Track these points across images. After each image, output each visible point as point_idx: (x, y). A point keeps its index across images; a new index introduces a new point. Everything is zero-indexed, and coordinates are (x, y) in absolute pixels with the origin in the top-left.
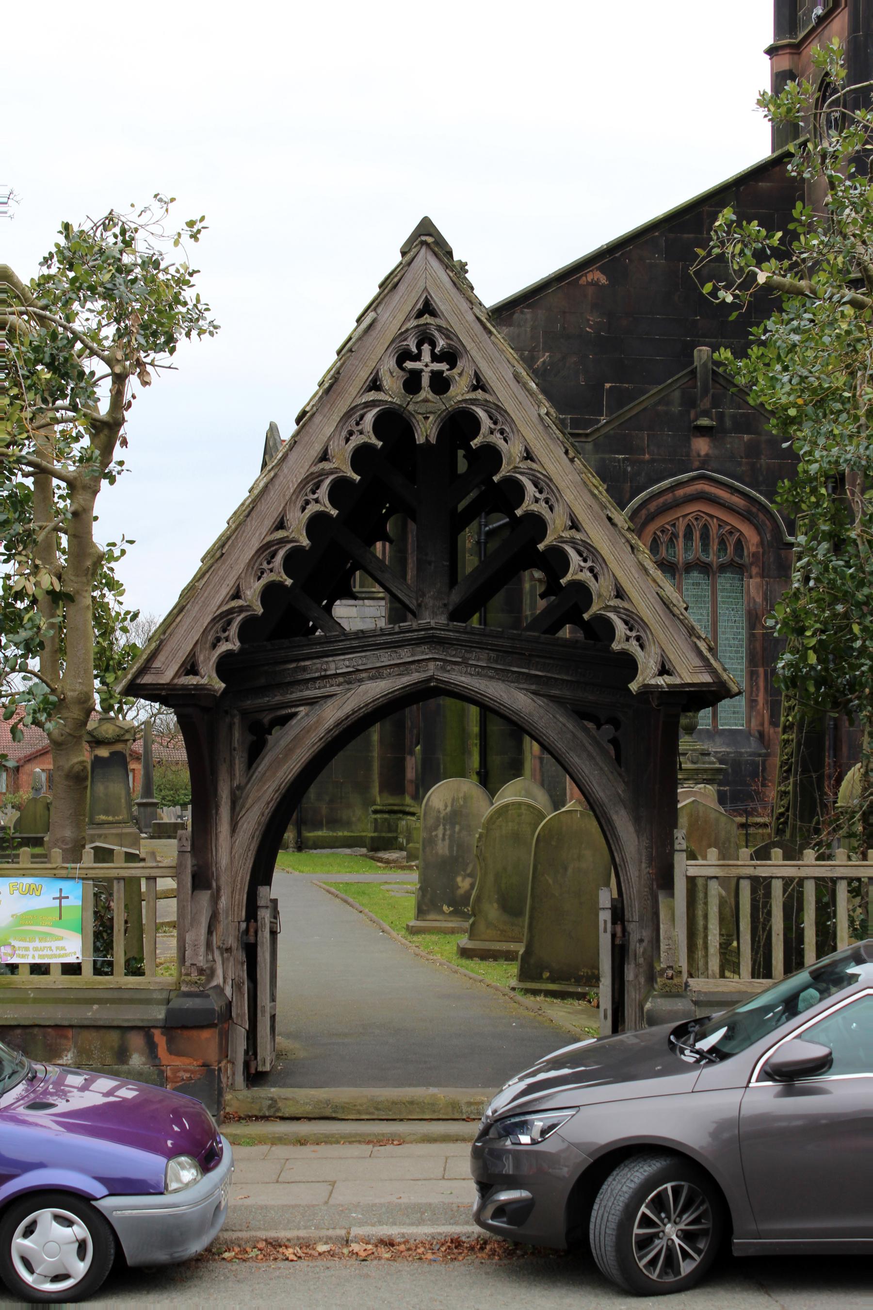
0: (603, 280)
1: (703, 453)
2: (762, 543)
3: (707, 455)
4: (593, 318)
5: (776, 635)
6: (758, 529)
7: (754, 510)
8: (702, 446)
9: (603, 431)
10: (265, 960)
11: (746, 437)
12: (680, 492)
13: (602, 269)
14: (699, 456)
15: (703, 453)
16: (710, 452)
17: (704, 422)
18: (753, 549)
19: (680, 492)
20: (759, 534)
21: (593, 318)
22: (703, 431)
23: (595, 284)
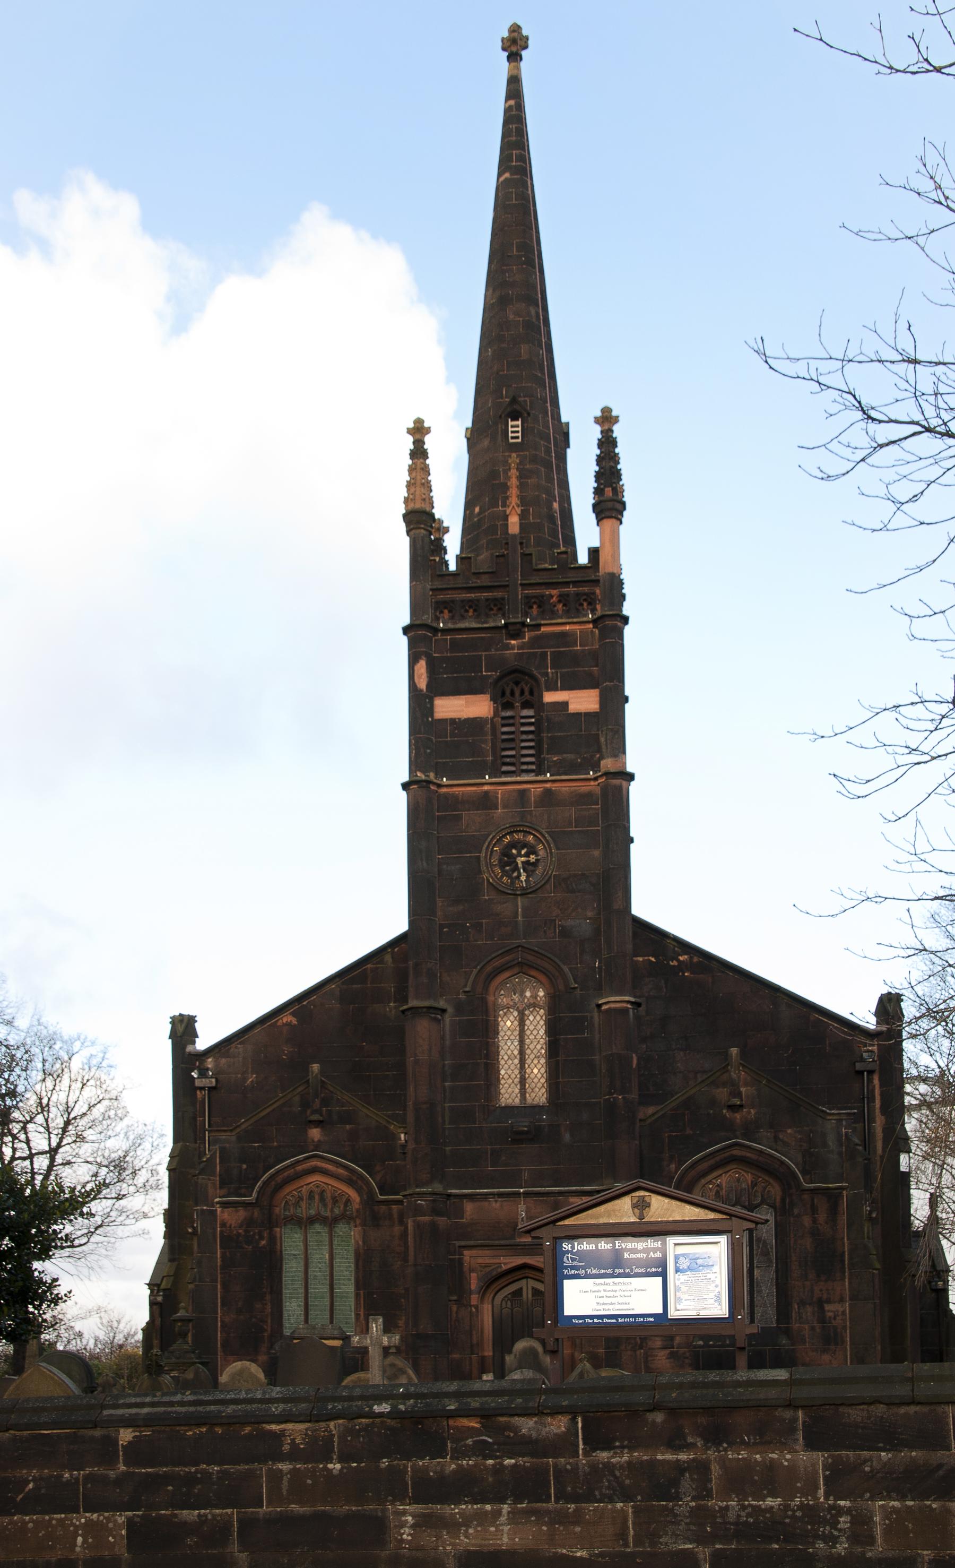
0: (294, 1021)
1: (316, 1140)
2: (361, 1202)
3: (319, 1141)
4: (287, 1049)
5: (31, 1308)
6: (359, 1191)
7: (355, 1178)
8: (315, 1133)
9: (243, 1127)
10: (694, 1385)
11: (348, 1127)
12: (299, 1168)
13: (293, 1014)
14: (313, 1141)
15: (316, 1140)
16: (322, 1139)
17: (316, 1117)
18: (357, 1206)
19: (299, 1168)
20: (360, 1195)
21: (287, 1049)
22: (318, 1124)
23: (288, 1024)
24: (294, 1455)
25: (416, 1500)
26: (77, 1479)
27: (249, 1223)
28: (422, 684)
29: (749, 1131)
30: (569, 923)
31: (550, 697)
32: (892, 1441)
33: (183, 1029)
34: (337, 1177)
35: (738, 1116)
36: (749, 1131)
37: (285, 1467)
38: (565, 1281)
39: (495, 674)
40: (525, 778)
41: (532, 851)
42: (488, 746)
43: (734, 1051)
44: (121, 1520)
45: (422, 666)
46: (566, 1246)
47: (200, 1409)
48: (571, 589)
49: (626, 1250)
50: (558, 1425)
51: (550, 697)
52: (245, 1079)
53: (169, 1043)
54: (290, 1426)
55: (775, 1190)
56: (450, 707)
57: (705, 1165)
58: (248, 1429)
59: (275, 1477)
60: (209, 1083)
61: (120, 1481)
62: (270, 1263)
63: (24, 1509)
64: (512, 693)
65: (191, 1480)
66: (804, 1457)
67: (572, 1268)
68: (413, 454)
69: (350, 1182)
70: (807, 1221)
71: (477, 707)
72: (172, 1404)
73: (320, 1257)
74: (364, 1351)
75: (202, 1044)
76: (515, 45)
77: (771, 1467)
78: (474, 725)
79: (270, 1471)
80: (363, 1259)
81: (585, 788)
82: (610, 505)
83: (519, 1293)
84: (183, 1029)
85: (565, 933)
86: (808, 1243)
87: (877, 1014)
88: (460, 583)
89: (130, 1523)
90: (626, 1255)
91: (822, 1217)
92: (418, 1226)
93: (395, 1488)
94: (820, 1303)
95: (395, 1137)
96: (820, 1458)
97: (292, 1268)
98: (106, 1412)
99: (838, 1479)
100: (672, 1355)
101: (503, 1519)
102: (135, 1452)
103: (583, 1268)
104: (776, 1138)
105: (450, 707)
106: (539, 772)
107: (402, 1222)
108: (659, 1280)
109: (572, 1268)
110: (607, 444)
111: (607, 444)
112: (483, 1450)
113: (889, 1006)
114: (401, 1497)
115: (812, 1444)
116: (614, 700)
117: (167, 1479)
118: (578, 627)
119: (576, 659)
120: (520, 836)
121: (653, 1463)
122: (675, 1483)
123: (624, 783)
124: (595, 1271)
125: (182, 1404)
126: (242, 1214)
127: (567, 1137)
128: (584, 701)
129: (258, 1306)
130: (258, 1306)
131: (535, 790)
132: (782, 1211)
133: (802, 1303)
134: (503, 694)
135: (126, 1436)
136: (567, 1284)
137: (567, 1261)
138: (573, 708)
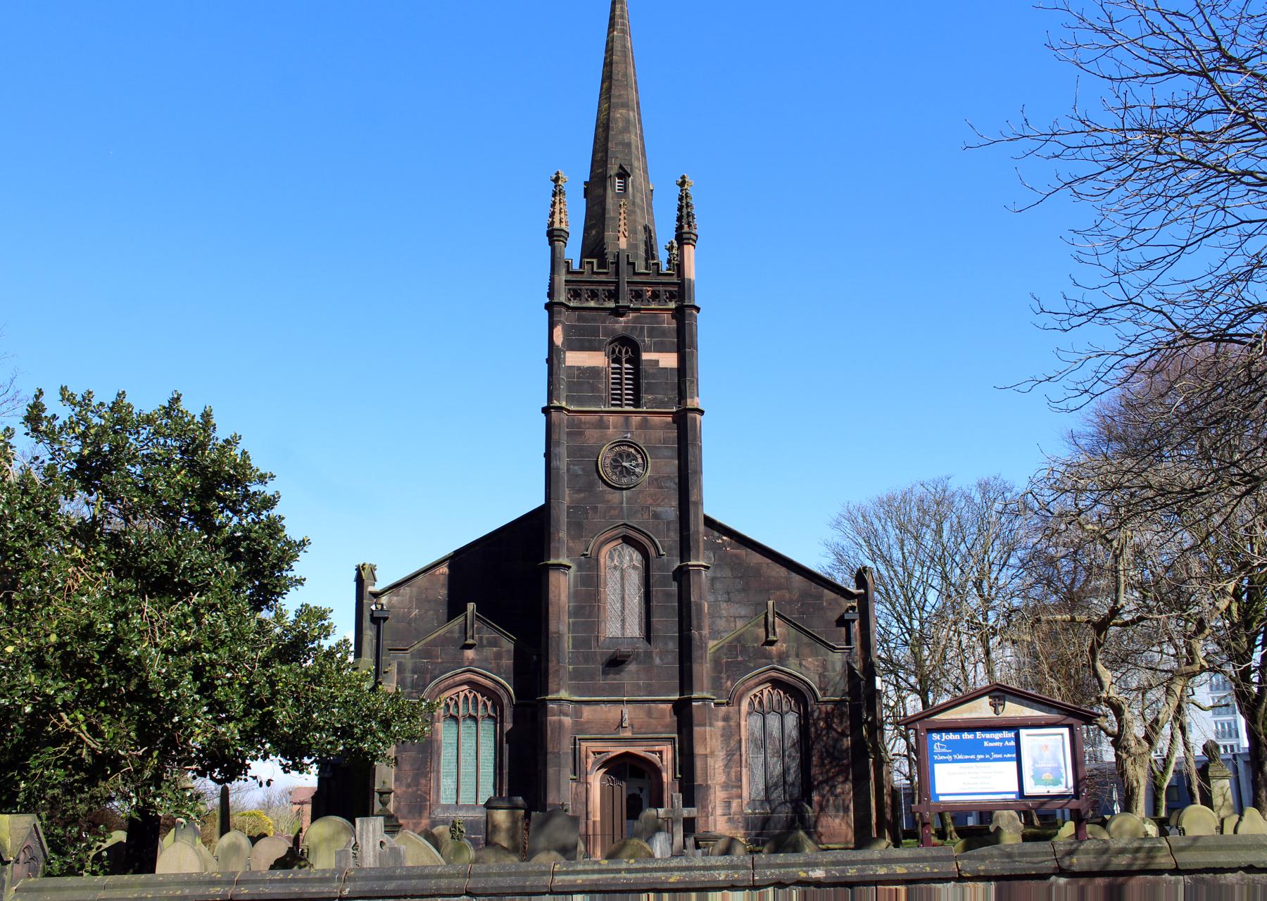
12: (457, 679)
19: (457, 679)
30: (659, 509)
35: (773, 648)
38: (937, 766)
39: (609, 340)
42: (602, 386)
46: (935, 736)
47: (647, 875)
49: (986, 739)
52: (410, 613)
53: (355, 584)
56: (575, 359)
57: (752, 682)
64: (620, 352)
67: (942, 754)
71: (597, 359)
72: (619, 871)
78: (593, 372)
85: (656, 516)
90: (986, 744)
98: (557, 878)
100: (730, 820)
103: (951, 754)
104: (801, 664)
108: (1014, 763)
109: (942, 754)
123: (698, 416)
124: (960, 757)
125: (629, 871)
127: (657, 661)
129: (423, 781)
130: (423, 781)
134: (614, 352)
137: (936, 749)
138: (661, 365)
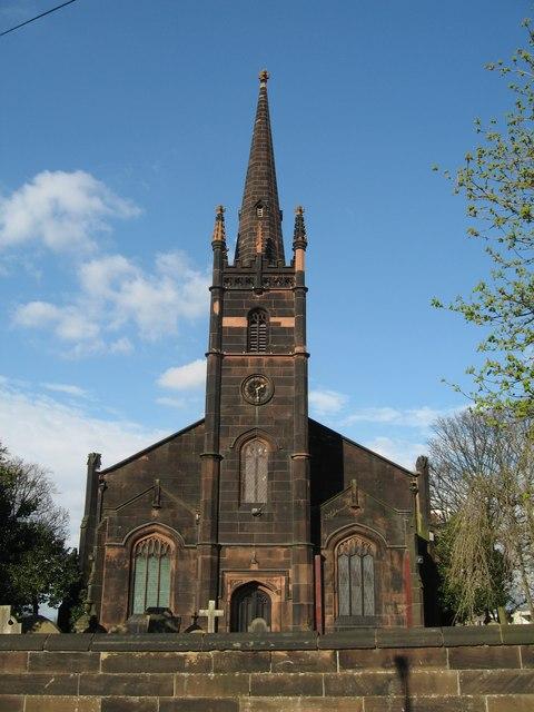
8: (155, 513)
12: (146, 530)
19: (146, 530)
24: (191, 669)
25: (253, 694)
26: (76, 678)
27: (120, 555)
28: (217, 311)
29: (361, 520)
31: (272, 320)
32: (493, 665)
33: (95, 460)
34: (164, 534)
36: (361, 520)
37: (186, 675)
40: (261, 353)
41: (259, 384)
42: (245, 340)
43: (354, 481)
44: (99, 699)
45: (217, 305)
48: (283, 276)
50: (327, 654)
51: (272, 320)
54: (189, 653)
55: (373, 547)
56: (228, 322)
58: (167, 654)
59: (180, 679)
60: (98, 481)
61: (99, 679)
62: (130, 577)
63: (47, 692)
65: (136, 680)
66: (450, 672)
68: (218, 219)
69: (170, 537)
70: (389, 563)
73: (153, 574)
74: (206, 618)
75: (103, 468)
76: (265, 79)
77: (433, 677)
79: (178, 678)
80: (176, 576)
81: (287, 359)
82: (301, 244)
83: (104, 607)
84: (95, 460)
86: (389, 574)
87: (417, 466)
88: (234, 270)
89: (103, 701)
91: (396, 562)
92: (203, 560)
93: (242, 687)
94: (396, 604)
95: (193, 516)
96: (458, 672)
97: (140, 580)
99: (466, 681)
101: (298, 704)
102: (108, 665)
105: (228, 322)
106: (268, 350)
107: (195, 557)
110: (300, 220)
111: (300, 220)
112: (288, 668)
113: (423, 463)
114: (245, 692)
115: (454, 666)
116: (302, 323)
117: (123, 679)
118: (288, 294)
119: (284, 305)
120: (256, 379)
121: (375, 676)
122: (386, 686)
126: (117, 551)
128: (288, 322)
131: (265, 359)
132: (378, 557)
133: (387, 604)
135: (104, 655)
136: (9, 607)
